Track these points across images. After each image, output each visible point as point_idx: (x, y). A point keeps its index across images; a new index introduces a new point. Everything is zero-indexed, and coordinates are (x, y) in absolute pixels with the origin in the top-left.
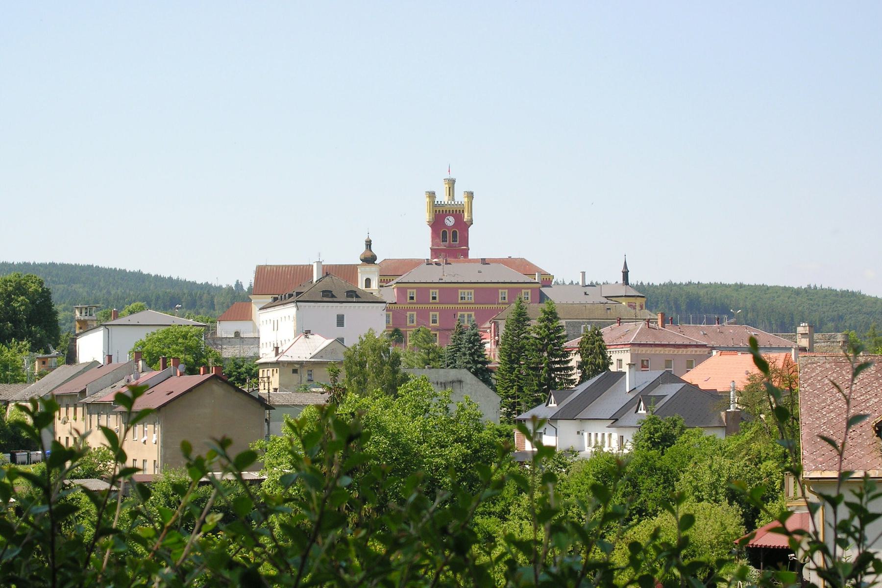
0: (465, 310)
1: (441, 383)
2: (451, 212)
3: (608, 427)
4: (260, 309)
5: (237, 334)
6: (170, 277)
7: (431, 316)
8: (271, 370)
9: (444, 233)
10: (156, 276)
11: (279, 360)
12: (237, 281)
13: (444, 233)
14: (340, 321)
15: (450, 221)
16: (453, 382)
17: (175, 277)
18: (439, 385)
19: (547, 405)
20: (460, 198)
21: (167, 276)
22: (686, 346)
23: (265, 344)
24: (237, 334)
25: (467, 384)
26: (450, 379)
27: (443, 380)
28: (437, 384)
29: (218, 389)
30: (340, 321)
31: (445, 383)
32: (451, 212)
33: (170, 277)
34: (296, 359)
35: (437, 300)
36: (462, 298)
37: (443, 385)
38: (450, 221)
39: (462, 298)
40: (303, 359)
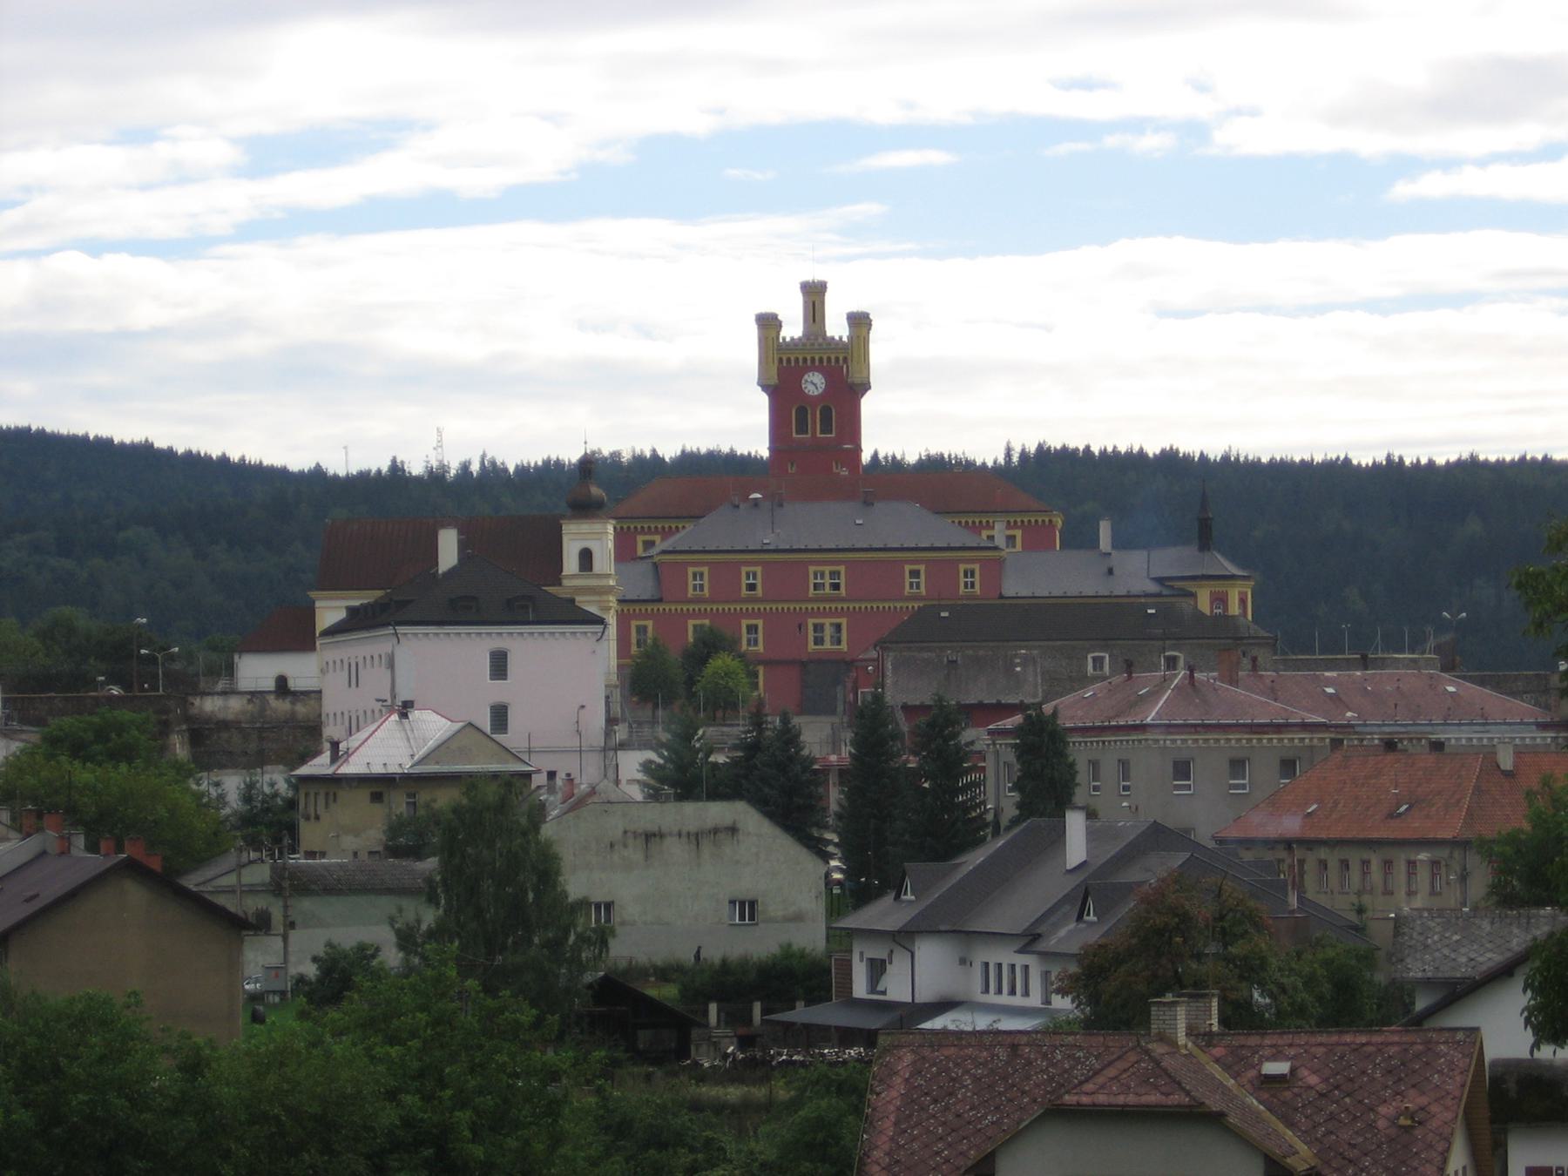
0: (825, 614)
1: (689, 834)
2: (817, 363)
3: (1015, 952)
4: (38, 895)
5: (282, 682)
6: (224, 455)
7: (811, 576)
8: (322, 792)
9: (802, 412)
10: (189, 454)
11: (339, 772)
12: (394, 461)
13: (802, 412)
14: (499, 665)
15: (814, 384)
16: (715, 831)
17: (235, 456)
18: (684, 839)
19: (897, 897)
20: (836, 327)
21: (215, 453)
22: (1278, 728)
23: (331, 717)
24: (282, 682)
25: (749, 834)
26: (709, 824)
27: (693, 828)
28: (680, 835)
29: (135, 895)
30: (499, 665)
31: (697, 834)
32: (817, 363)
33: (224, 455)
34: (377, 769)
35: (759, 592)
36: (816, 586)
37: (693, 839)
38: (814, 384)
39: (816, 586)
40: (393, 769)
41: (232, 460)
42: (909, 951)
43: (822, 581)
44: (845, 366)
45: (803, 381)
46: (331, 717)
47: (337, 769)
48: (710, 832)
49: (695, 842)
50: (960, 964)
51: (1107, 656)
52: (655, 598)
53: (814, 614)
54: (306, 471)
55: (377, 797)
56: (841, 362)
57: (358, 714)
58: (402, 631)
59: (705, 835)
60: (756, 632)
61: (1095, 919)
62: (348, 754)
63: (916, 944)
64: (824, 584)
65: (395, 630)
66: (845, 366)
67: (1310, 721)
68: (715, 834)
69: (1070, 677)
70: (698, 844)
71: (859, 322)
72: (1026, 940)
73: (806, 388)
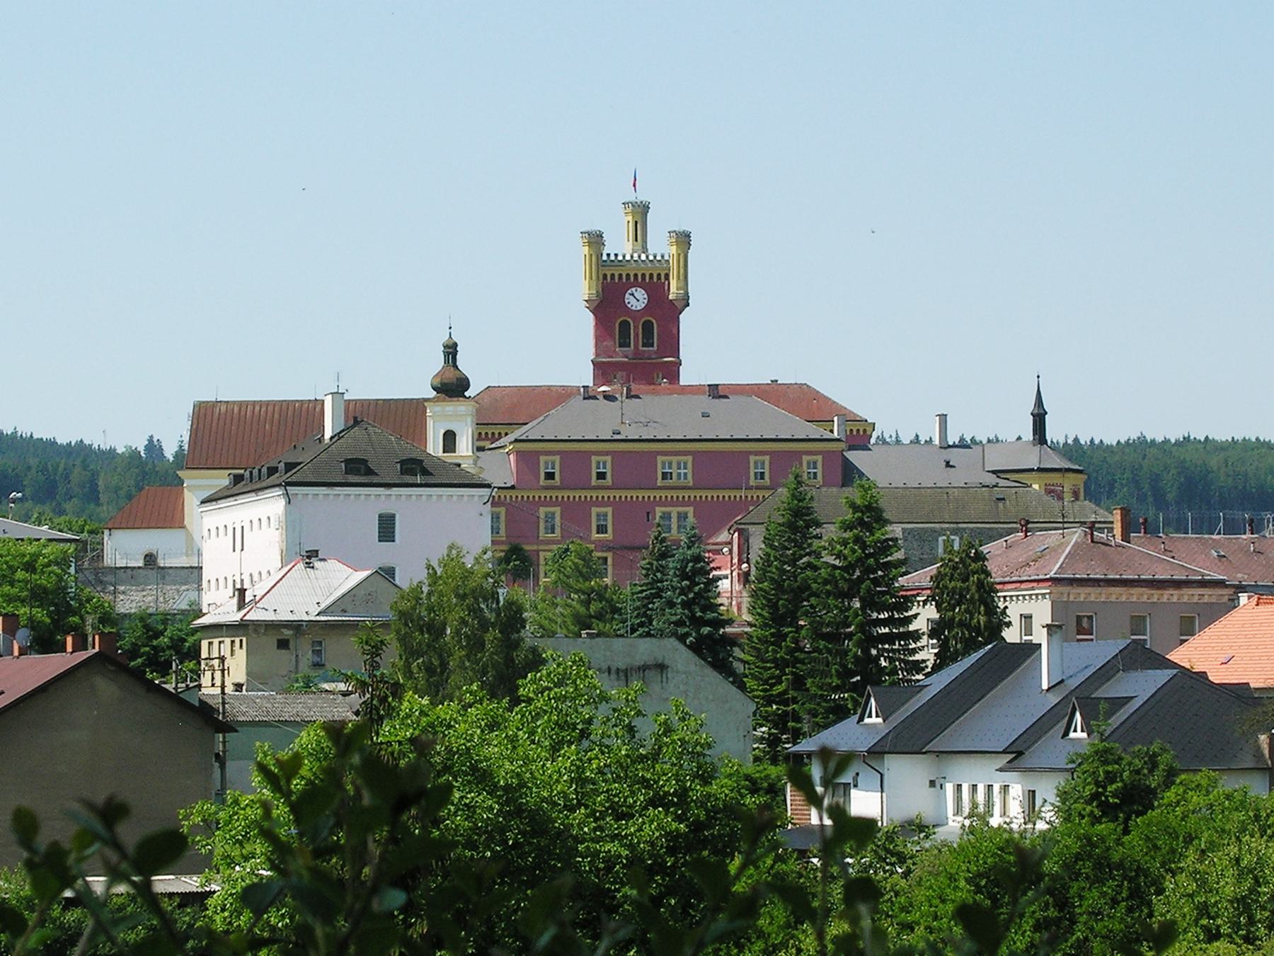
3: (1001, 770)
5: (150, 559)
8: (228, 641)
12: (151, 439)
13: (625, 326)
14: (387, 528)
15: (637, 299)
16: (644, 668)
18: (613, 676)
19: (861, 719)
20: (660, 245)
22: (1178, 584)
23: (213, 582)
24: (150, 559)
25: (678, 672)
26: (639, 660)
27: (622, 666)
29: (105, 687)
30: (387, 528)
36: (665, 476)
38: (637, 299)
39: (665, 476)
41: (5, 433)
42: (879, 772)
43: (670, 471)
44: (667, 282)
45: (630, 291)
46: (213, 582)
47: (245, 615)
48: (639, 668)
49: (623, 678)
50: (930, 786)
51: (958, 539)
52: (509, 485)
53: (661, 503)
54: (73, 444)
55: (283, 644)
56: (663, 277)
57: (234, 578)
58: (293, 492)
59: (634, 672)
60: (598, 526)
61: (1085, 735)
62: (255, 601)
63: (886, 761)
64: (671, 473)
65: (286, 490)
66: (667, 282)
67: (1209, 578)
68: (644, 671)
69: (921, 559)
70: (627, 681)
71: (683, 240)
72: (1012, 756)
73: (629, 303)
